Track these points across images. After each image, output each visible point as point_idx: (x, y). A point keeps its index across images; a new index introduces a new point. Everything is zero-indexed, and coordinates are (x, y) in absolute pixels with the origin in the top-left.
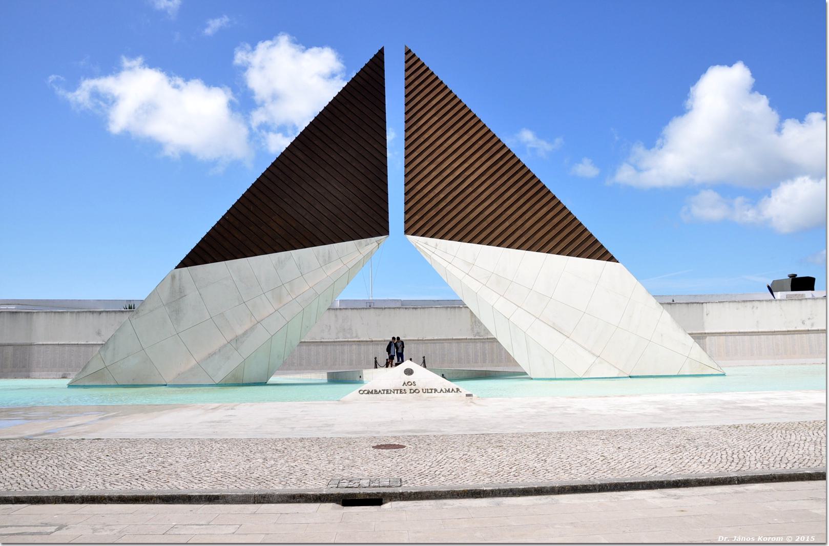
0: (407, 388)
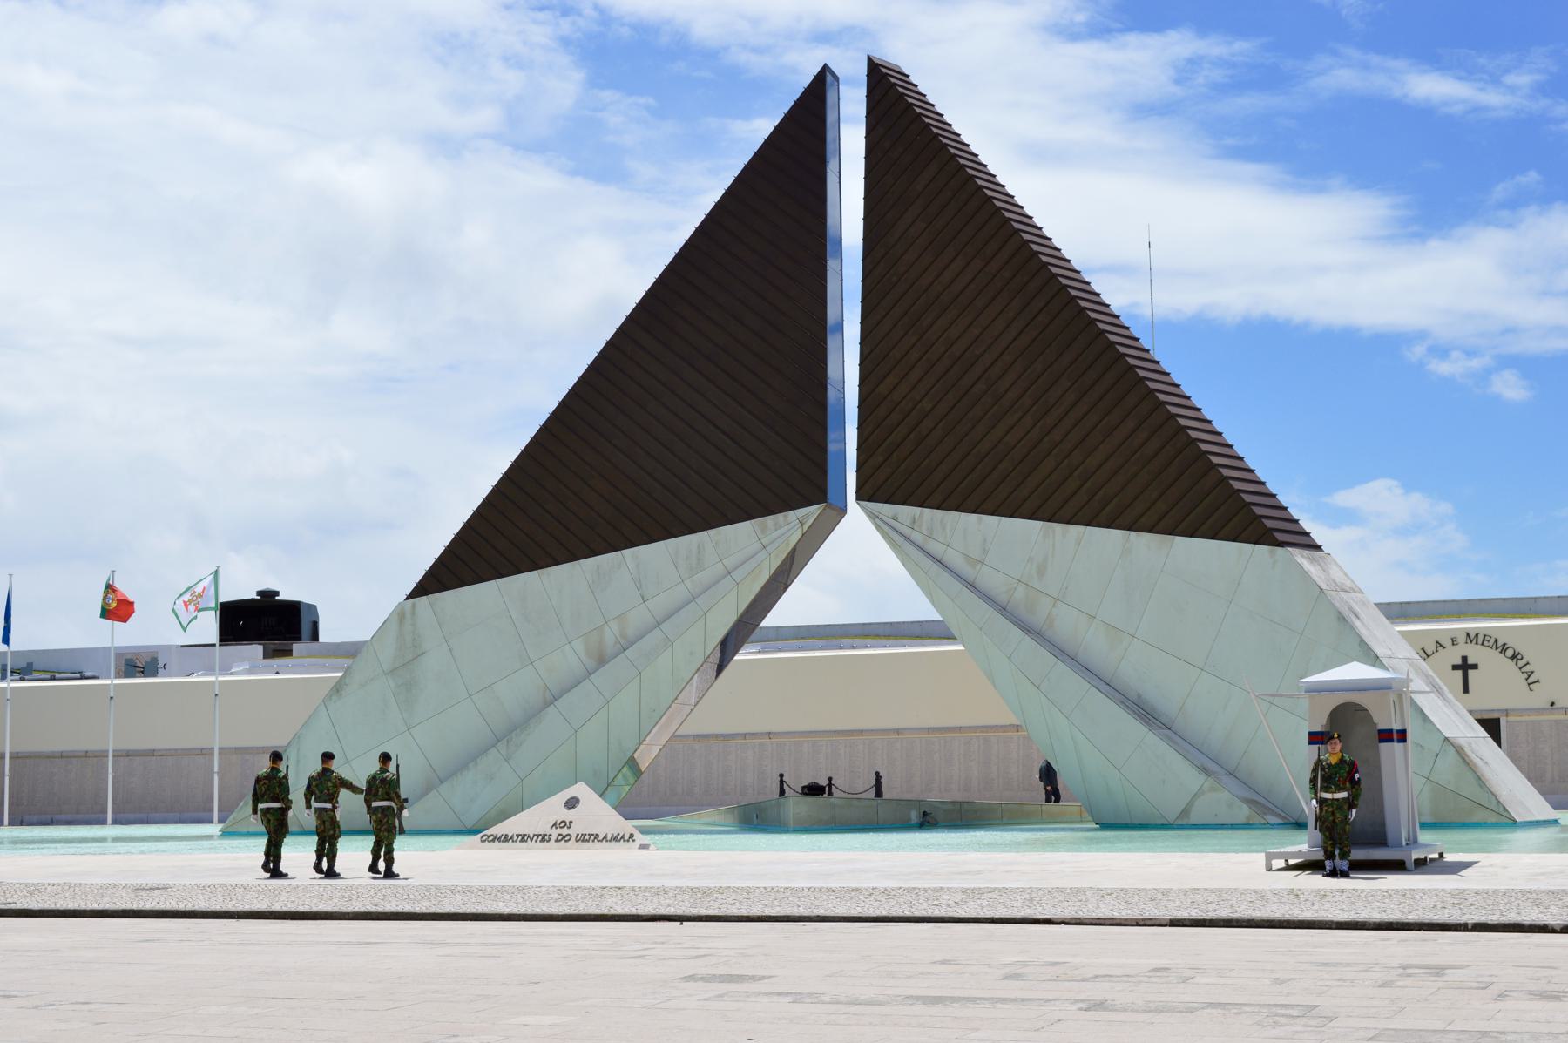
0: (555, 833)
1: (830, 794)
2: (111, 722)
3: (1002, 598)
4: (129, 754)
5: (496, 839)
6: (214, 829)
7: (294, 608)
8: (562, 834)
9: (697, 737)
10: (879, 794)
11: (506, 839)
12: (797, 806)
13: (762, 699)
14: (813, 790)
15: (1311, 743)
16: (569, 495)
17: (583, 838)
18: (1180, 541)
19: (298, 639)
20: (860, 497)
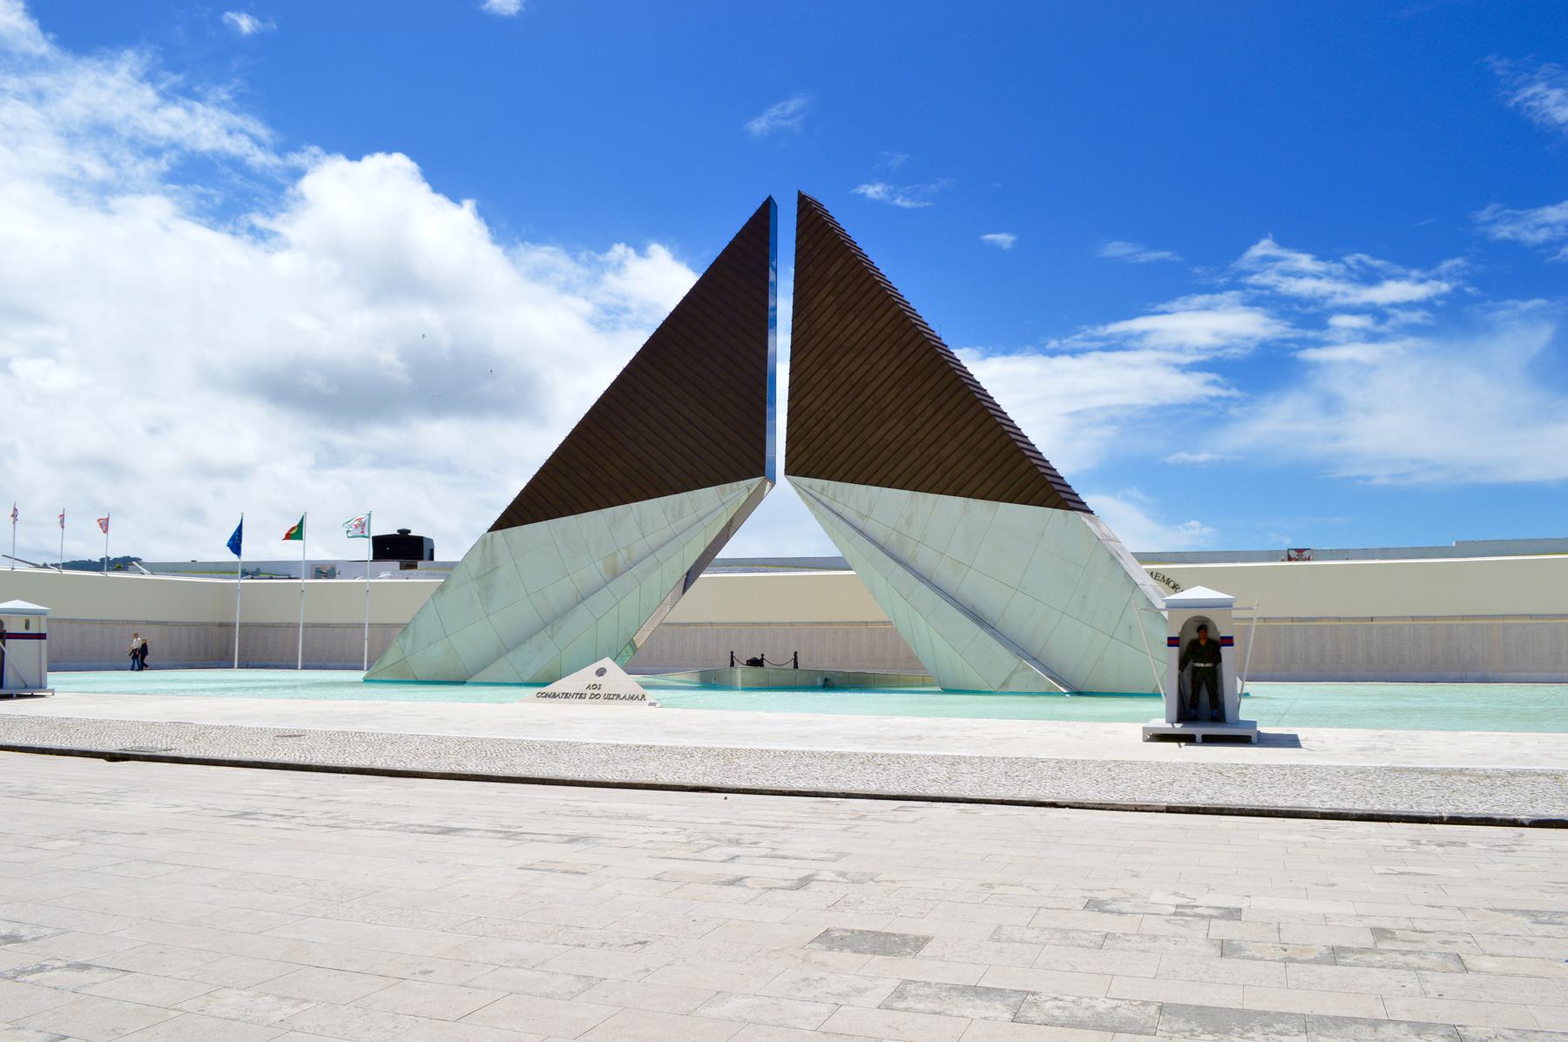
0: (589, 692)
2: (302, 606)
3: (882, 541)
4: (314, 626)
5: (547, 696)
6: (359, 676)
7: (419, 541)
8: (594, 694)
10: (796, 666)
11: (555, 696)
12: (740, 673)
13: (715, 598)
14: (756, 663)
15: (1170, 645)
16: (590, 471)
17: (609, 697)
18: (1003, 505)
19: (421, 558)
20: (790, 470)
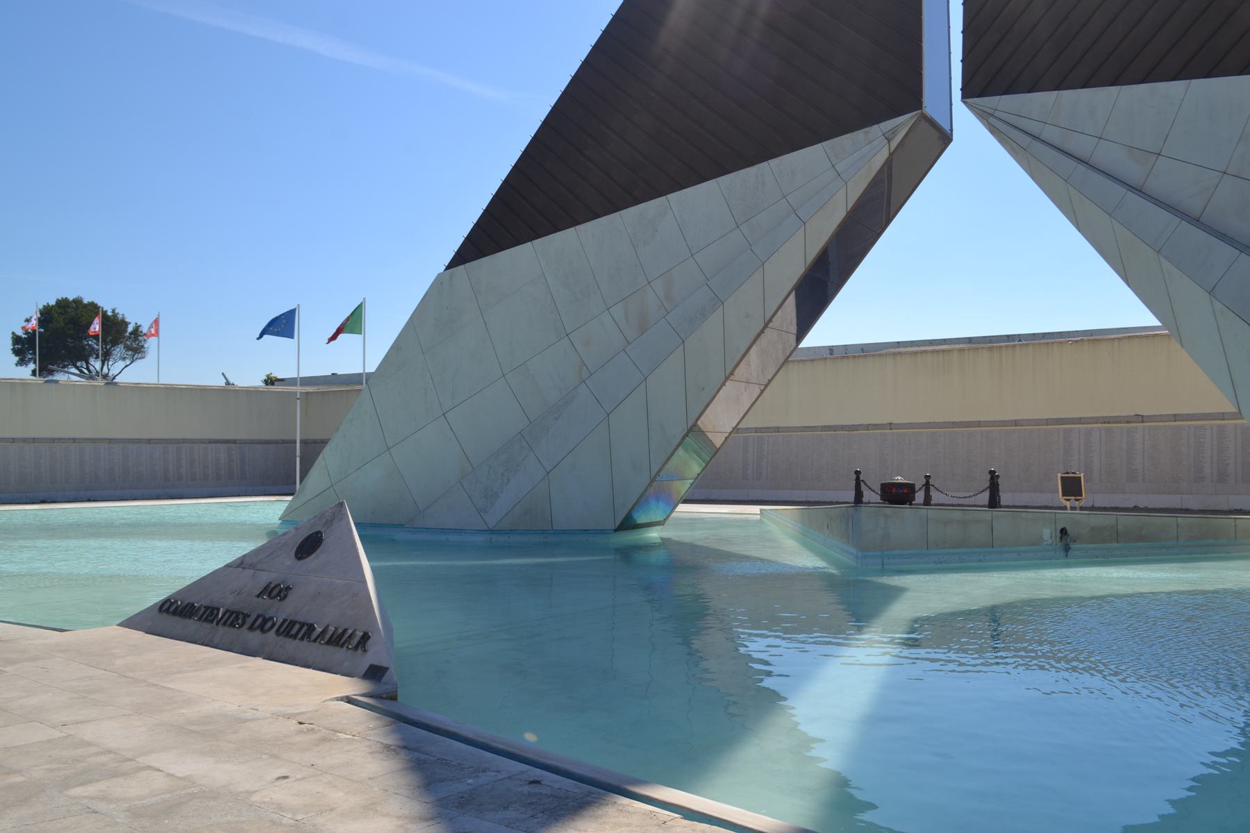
1: (927, 501)
9: (757, 430)
14: (897, 495)
20: (967, 93)
